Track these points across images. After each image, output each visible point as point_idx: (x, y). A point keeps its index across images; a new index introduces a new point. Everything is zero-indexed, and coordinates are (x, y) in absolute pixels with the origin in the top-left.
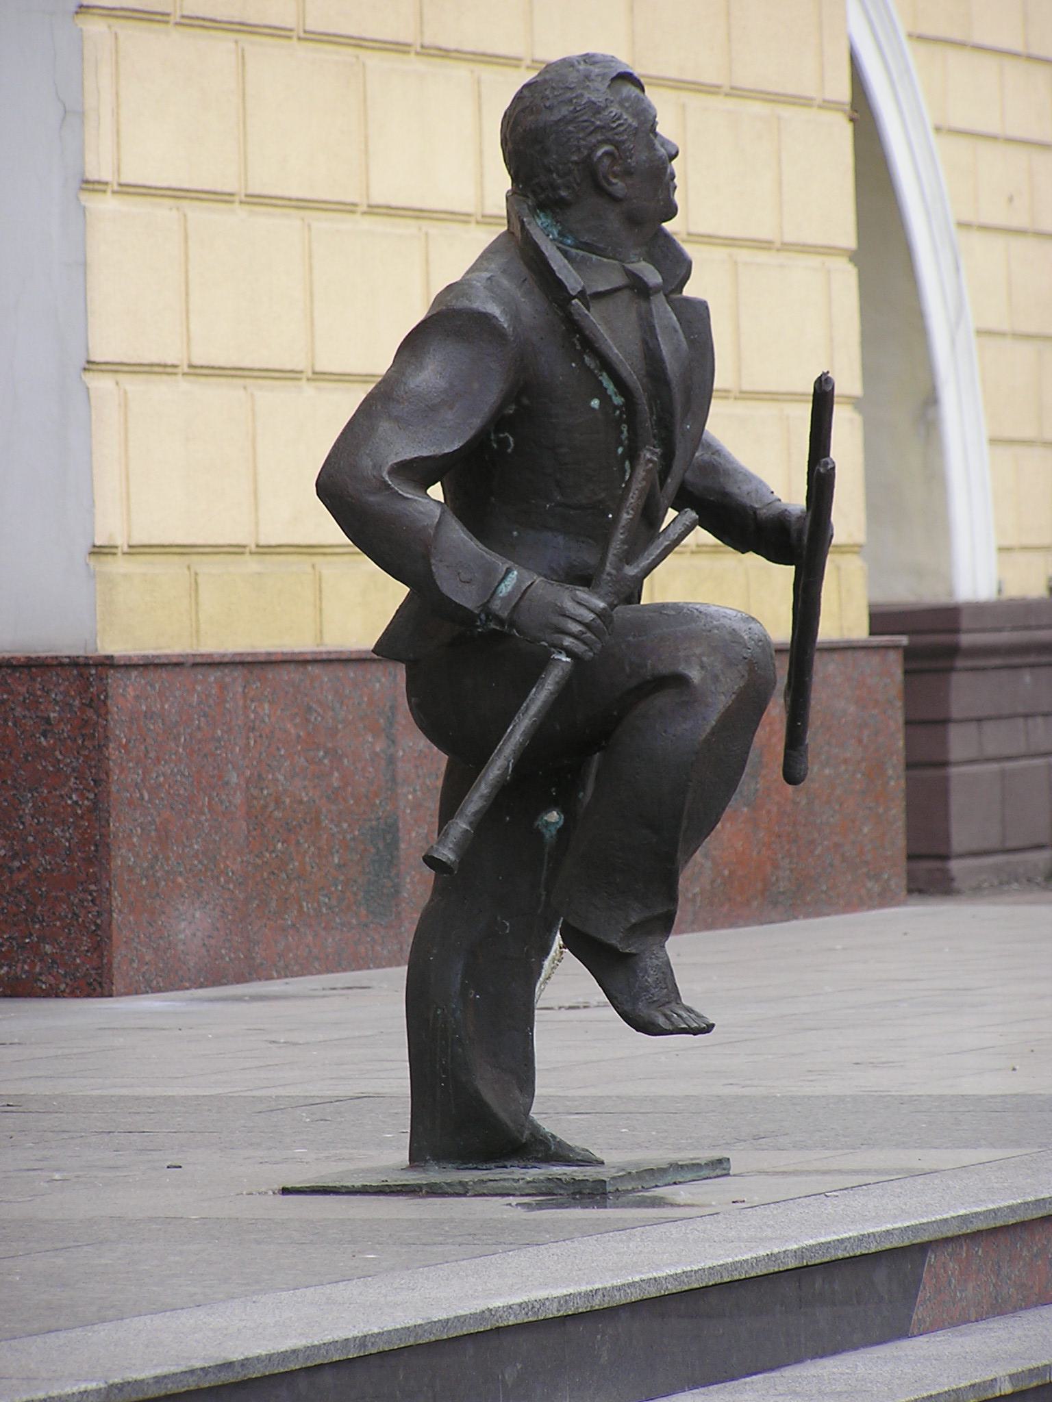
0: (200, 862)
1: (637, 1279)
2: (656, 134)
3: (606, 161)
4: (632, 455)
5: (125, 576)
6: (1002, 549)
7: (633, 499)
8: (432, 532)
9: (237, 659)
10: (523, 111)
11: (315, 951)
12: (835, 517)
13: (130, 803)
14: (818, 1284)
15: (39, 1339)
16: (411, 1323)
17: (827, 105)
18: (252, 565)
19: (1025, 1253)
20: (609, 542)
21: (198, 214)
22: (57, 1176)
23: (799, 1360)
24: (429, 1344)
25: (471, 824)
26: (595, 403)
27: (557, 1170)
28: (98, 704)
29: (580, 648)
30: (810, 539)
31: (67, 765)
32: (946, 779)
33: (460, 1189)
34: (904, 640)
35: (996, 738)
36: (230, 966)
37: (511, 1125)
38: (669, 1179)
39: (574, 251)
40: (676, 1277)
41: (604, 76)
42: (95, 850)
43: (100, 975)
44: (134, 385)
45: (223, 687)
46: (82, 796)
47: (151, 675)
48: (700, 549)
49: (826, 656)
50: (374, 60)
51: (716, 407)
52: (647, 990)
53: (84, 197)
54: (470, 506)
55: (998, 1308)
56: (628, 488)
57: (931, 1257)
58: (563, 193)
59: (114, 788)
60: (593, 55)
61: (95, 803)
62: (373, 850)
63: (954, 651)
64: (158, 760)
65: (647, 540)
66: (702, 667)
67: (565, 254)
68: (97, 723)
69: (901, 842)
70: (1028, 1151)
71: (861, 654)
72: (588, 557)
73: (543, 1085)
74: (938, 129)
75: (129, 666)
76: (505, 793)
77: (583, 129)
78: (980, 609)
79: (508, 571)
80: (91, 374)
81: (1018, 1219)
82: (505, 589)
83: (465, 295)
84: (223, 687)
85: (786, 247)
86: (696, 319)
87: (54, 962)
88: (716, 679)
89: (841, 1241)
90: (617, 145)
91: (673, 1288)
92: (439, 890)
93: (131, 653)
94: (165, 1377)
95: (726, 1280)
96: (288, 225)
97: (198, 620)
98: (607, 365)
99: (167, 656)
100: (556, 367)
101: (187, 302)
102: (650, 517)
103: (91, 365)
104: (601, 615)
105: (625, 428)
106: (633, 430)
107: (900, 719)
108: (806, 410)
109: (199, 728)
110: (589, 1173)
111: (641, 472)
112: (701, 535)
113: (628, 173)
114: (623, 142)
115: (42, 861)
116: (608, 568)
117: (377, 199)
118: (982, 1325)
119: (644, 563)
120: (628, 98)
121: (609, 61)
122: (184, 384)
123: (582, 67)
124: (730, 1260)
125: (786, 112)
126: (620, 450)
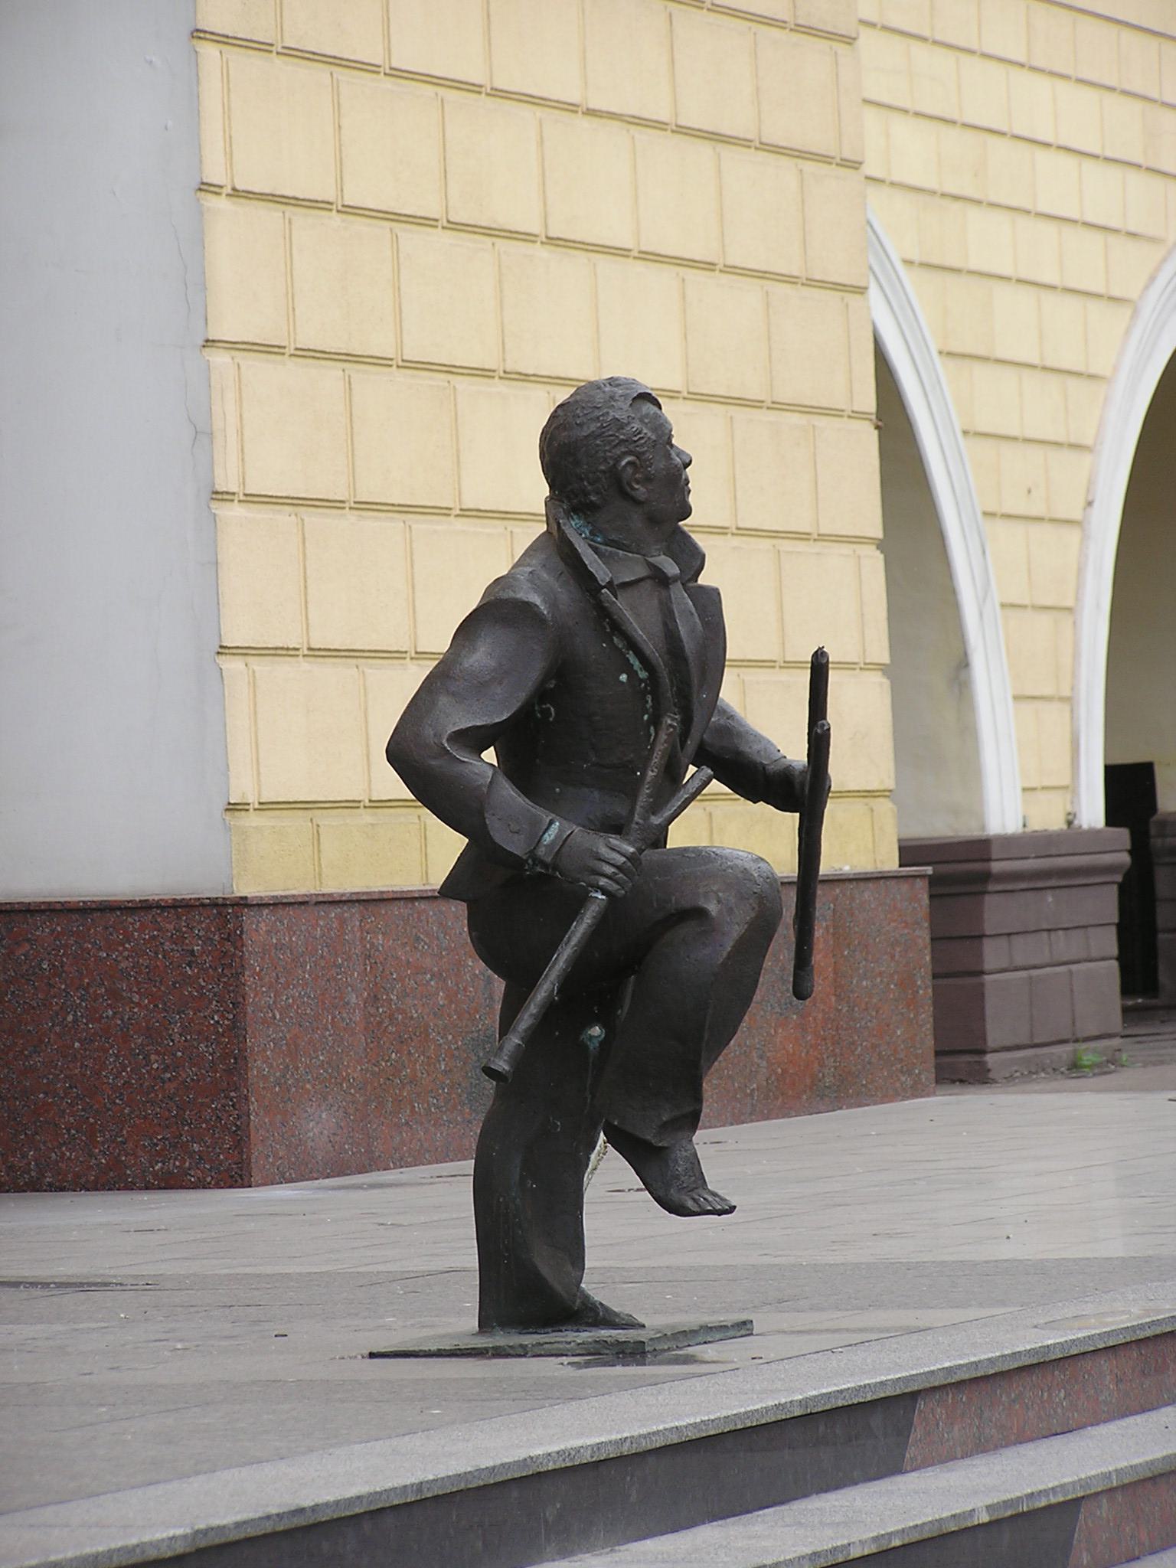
0: (326, 1071)
1: (661, 1427)
2: (672, 446)
3: (630, 470)
4: (656, 721)
5: (256, 828)
6: (1024, 790)
7: (656, 759)
8: (485, 790)
9: (354, 898)
10: (557, 428)
11: (426, 1145)
12: (832, 770)
13: (264, 1021)
14: (822, 1428)
15: (140, 1492)
16: (462, 1470)
17: (856, 415)
18: (366, 817)
19: (1004, 1398)
20: (637, 793)
21: (313, 518)
22: (179, 1346)
23: (805, 1495)
24: (478, 1488)
25: (522, 1039)
26: (624, 677)
27: (604, 1333)
28: (235, 938)
29: (613, 887)
30: (810, 789)
31: (209, 991)
32: (982, 985)
33: (521, 1351)
34: (929, 870)
35: (1024, 950)
36: (352, 1159)
37: (565, 1295)
38: (700, 1339)
39: (603, 547)
40: (695, 1425)
41: (625, 396)
42: (233, 1065)
43: (241, 1169)
44: (259, 665)
45: (342, 922)
46: (222, 1016)
47: (281, 912)
48: (716, 797)
49: (826, 887)
50: (462, 383)
51: (729, 676)
52: (677, 1177)
53: (214, 505)
54: (519, 768)
55: (982, 1446)
56: (652, 750)
57: (921, 1404)
58: (593, 498)
59: (250, 1010)
60: (617, 379)
61: (234, 1021)
62: (475, 1058)
63: (986, 877)
64: (287, 986)
65: (670, 792)
66: (719, 902)
67: (596, 550)
68: (234, 955)
69: (930, 1042)
70: (1010, 1310)
71: (893, 882)
72: (619, 808)
73: (592, 1260)
74: (965, 433)
75: (261, 905)
76: (551, 1012)
77: (609, 443)
78: (1008, 840)
79: (551, 822)
80: (224, 657)
81: (996, 1370)
82: (548, 838)
83: (510, 587)
84: (342, 922)
85: (822, 538)
86: (709, 603)
87: (201, 1158)
88: (730, 910)
89: (841, 1392)
90: (638, 455)
91: (693, 1435)
92: (500, 1095)
93: (263, 894)
94: (245, 1522)
95: (739, 1427)
96: (391, 527)
97: (320, 865)
98: (633, 645)
99: (293, 896)
100: (590, 647)
101: (306, 594)
102: (672, 774)
103: (223, 650)
104: (630, 858)
105: (649, 698)
106: (656, 700)
107: (928, 940)
108: (806, 676)
109: (322, 957)
110: (631, 1335)
111: (663, 737)
112: (716, 786)
113: (648, 479)
114: (644, 453)
115: (189, 1073)
116: (636, 818)
117: (469, 504)
118: (967, 1461)
119: (667, 813)
120: (647, 415)
121: (631, 383)
122: (305, 665)
123: (608, 389)
124: (743, 1410)
125: (821, 422)
126: (646, 717)
